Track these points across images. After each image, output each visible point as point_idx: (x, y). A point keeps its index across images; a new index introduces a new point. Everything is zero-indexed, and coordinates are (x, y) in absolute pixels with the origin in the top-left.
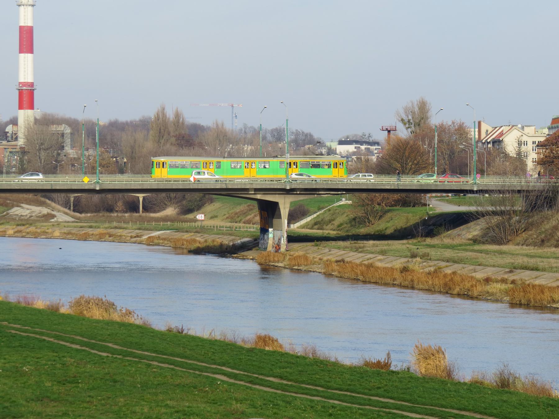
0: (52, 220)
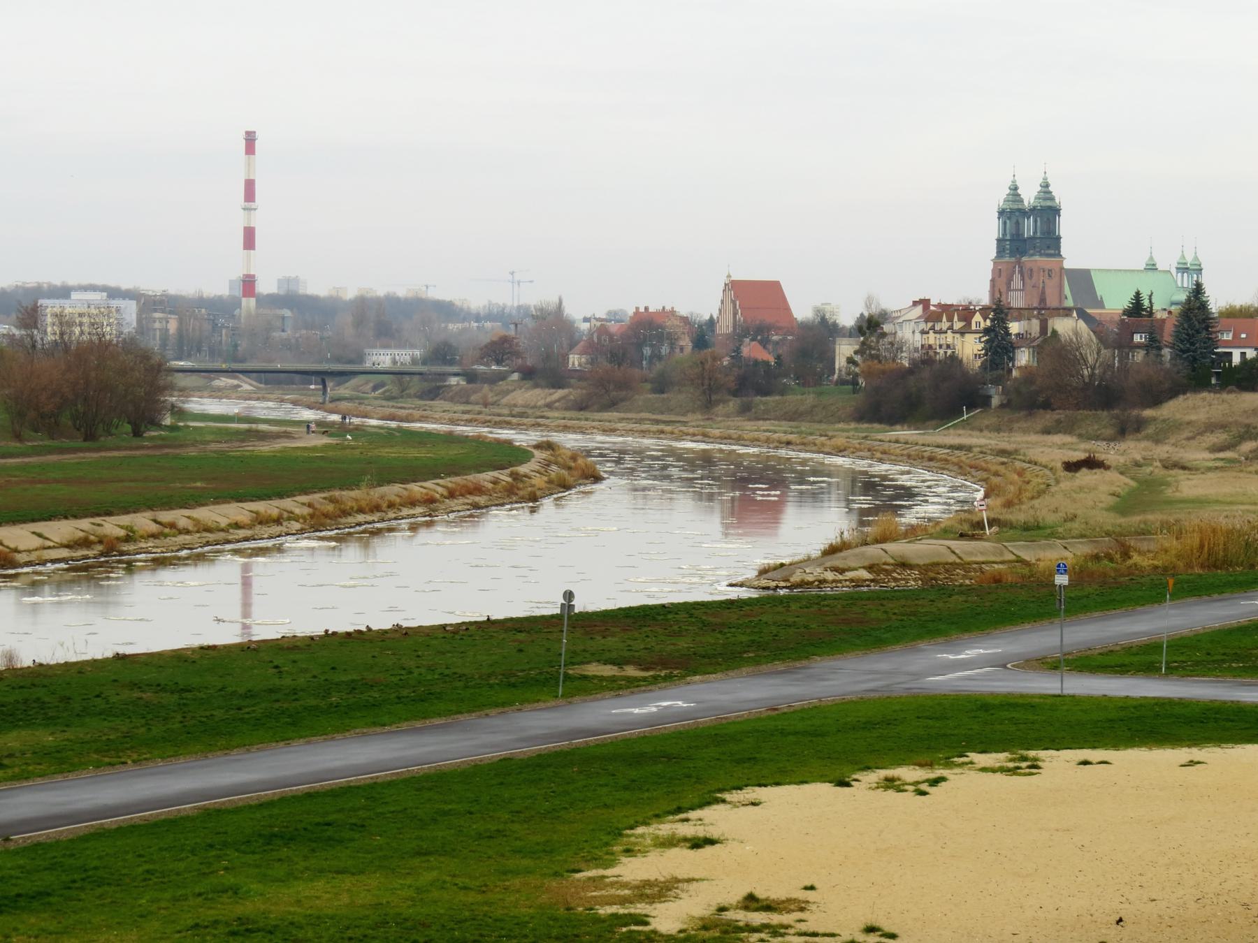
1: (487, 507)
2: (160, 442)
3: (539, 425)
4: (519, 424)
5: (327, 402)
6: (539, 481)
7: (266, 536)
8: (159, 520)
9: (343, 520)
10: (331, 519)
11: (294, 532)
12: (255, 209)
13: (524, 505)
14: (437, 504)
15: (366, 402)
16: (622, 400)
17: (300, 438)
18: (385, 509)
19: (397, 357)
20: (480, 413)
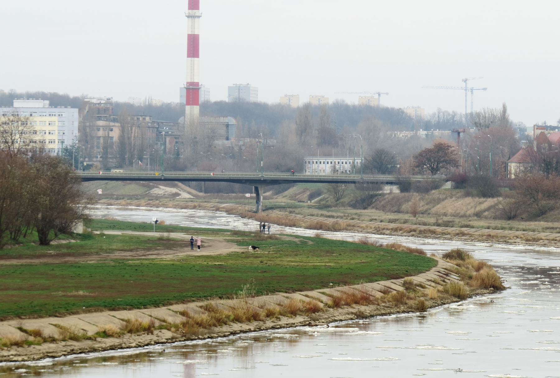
0: (178, 197)
1: (372, 316)
2: (64, 251)
3: (463, 234)
4: (443, 234)
5: (260, 210)
6: (431, 291)
7: (133, 345)
8: (25, 327)
9: (217, 329)
10: (205, 328)
11: (164, 340)
12: (199, 17)
13: (411, 314)
14: (320, 313)
15: (297, 211)
16: (552, 209)
17: (210, 246)
18: (264, 318)
19: (337, 167)
20: (405, 222)
